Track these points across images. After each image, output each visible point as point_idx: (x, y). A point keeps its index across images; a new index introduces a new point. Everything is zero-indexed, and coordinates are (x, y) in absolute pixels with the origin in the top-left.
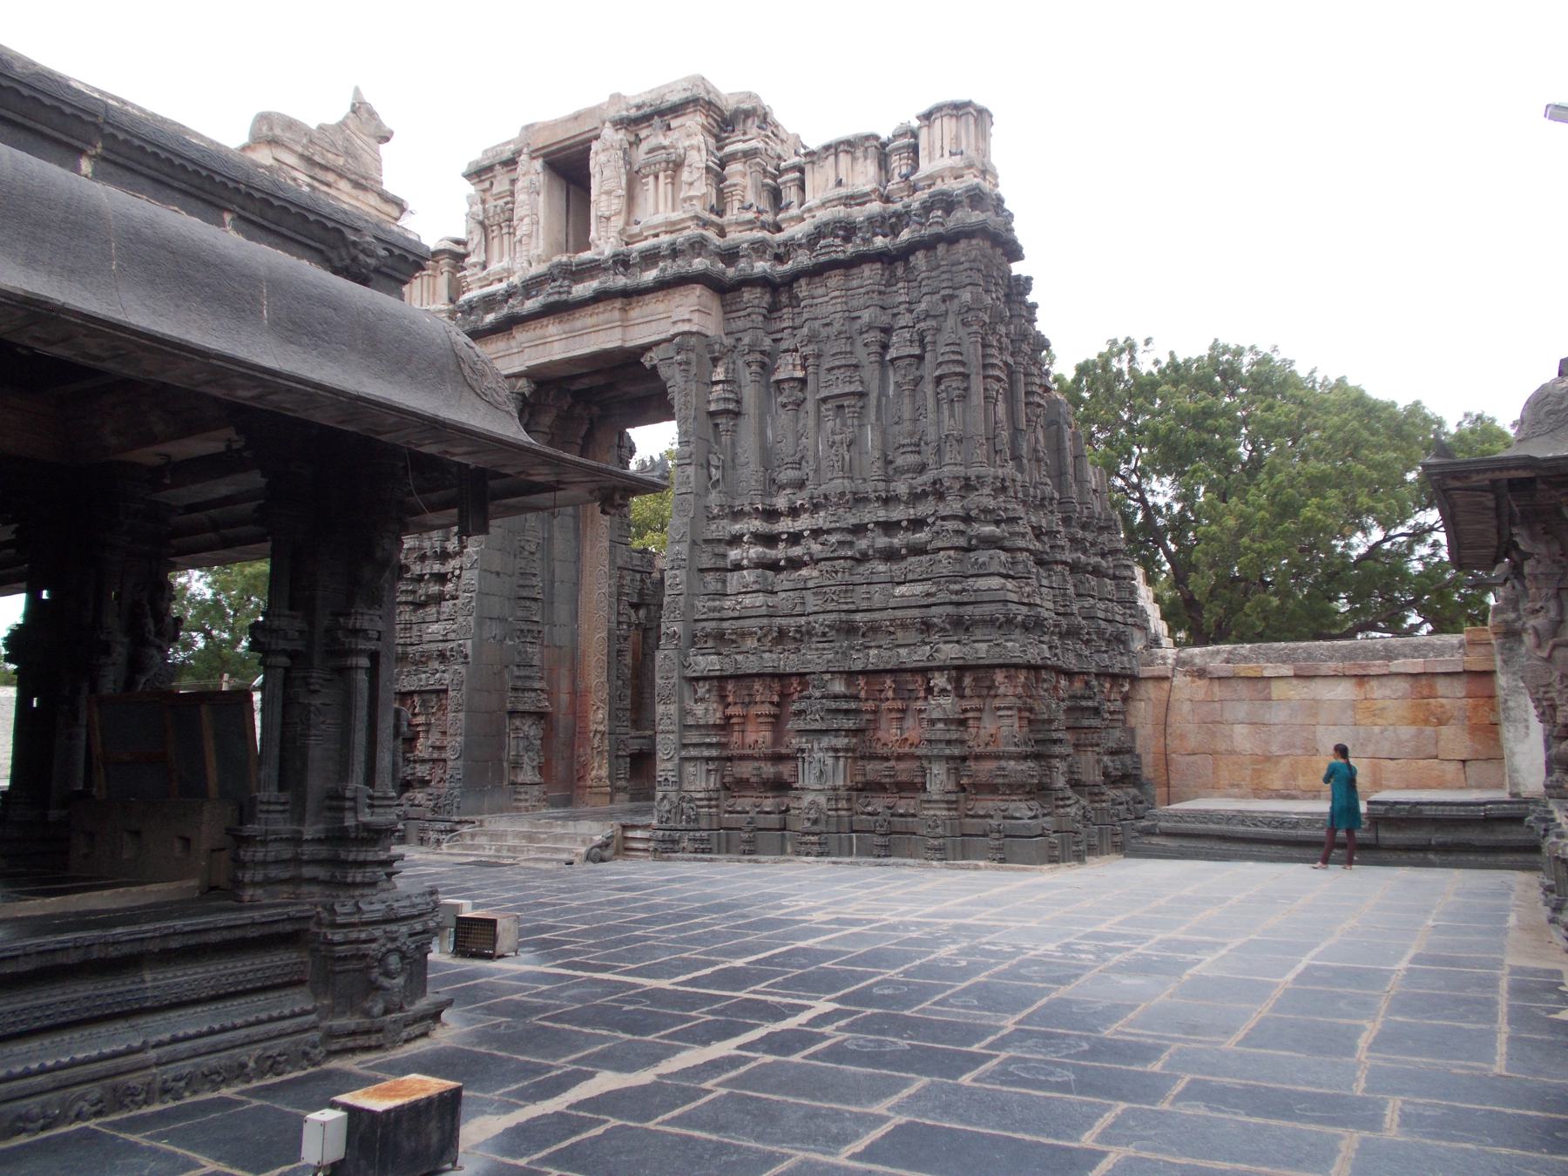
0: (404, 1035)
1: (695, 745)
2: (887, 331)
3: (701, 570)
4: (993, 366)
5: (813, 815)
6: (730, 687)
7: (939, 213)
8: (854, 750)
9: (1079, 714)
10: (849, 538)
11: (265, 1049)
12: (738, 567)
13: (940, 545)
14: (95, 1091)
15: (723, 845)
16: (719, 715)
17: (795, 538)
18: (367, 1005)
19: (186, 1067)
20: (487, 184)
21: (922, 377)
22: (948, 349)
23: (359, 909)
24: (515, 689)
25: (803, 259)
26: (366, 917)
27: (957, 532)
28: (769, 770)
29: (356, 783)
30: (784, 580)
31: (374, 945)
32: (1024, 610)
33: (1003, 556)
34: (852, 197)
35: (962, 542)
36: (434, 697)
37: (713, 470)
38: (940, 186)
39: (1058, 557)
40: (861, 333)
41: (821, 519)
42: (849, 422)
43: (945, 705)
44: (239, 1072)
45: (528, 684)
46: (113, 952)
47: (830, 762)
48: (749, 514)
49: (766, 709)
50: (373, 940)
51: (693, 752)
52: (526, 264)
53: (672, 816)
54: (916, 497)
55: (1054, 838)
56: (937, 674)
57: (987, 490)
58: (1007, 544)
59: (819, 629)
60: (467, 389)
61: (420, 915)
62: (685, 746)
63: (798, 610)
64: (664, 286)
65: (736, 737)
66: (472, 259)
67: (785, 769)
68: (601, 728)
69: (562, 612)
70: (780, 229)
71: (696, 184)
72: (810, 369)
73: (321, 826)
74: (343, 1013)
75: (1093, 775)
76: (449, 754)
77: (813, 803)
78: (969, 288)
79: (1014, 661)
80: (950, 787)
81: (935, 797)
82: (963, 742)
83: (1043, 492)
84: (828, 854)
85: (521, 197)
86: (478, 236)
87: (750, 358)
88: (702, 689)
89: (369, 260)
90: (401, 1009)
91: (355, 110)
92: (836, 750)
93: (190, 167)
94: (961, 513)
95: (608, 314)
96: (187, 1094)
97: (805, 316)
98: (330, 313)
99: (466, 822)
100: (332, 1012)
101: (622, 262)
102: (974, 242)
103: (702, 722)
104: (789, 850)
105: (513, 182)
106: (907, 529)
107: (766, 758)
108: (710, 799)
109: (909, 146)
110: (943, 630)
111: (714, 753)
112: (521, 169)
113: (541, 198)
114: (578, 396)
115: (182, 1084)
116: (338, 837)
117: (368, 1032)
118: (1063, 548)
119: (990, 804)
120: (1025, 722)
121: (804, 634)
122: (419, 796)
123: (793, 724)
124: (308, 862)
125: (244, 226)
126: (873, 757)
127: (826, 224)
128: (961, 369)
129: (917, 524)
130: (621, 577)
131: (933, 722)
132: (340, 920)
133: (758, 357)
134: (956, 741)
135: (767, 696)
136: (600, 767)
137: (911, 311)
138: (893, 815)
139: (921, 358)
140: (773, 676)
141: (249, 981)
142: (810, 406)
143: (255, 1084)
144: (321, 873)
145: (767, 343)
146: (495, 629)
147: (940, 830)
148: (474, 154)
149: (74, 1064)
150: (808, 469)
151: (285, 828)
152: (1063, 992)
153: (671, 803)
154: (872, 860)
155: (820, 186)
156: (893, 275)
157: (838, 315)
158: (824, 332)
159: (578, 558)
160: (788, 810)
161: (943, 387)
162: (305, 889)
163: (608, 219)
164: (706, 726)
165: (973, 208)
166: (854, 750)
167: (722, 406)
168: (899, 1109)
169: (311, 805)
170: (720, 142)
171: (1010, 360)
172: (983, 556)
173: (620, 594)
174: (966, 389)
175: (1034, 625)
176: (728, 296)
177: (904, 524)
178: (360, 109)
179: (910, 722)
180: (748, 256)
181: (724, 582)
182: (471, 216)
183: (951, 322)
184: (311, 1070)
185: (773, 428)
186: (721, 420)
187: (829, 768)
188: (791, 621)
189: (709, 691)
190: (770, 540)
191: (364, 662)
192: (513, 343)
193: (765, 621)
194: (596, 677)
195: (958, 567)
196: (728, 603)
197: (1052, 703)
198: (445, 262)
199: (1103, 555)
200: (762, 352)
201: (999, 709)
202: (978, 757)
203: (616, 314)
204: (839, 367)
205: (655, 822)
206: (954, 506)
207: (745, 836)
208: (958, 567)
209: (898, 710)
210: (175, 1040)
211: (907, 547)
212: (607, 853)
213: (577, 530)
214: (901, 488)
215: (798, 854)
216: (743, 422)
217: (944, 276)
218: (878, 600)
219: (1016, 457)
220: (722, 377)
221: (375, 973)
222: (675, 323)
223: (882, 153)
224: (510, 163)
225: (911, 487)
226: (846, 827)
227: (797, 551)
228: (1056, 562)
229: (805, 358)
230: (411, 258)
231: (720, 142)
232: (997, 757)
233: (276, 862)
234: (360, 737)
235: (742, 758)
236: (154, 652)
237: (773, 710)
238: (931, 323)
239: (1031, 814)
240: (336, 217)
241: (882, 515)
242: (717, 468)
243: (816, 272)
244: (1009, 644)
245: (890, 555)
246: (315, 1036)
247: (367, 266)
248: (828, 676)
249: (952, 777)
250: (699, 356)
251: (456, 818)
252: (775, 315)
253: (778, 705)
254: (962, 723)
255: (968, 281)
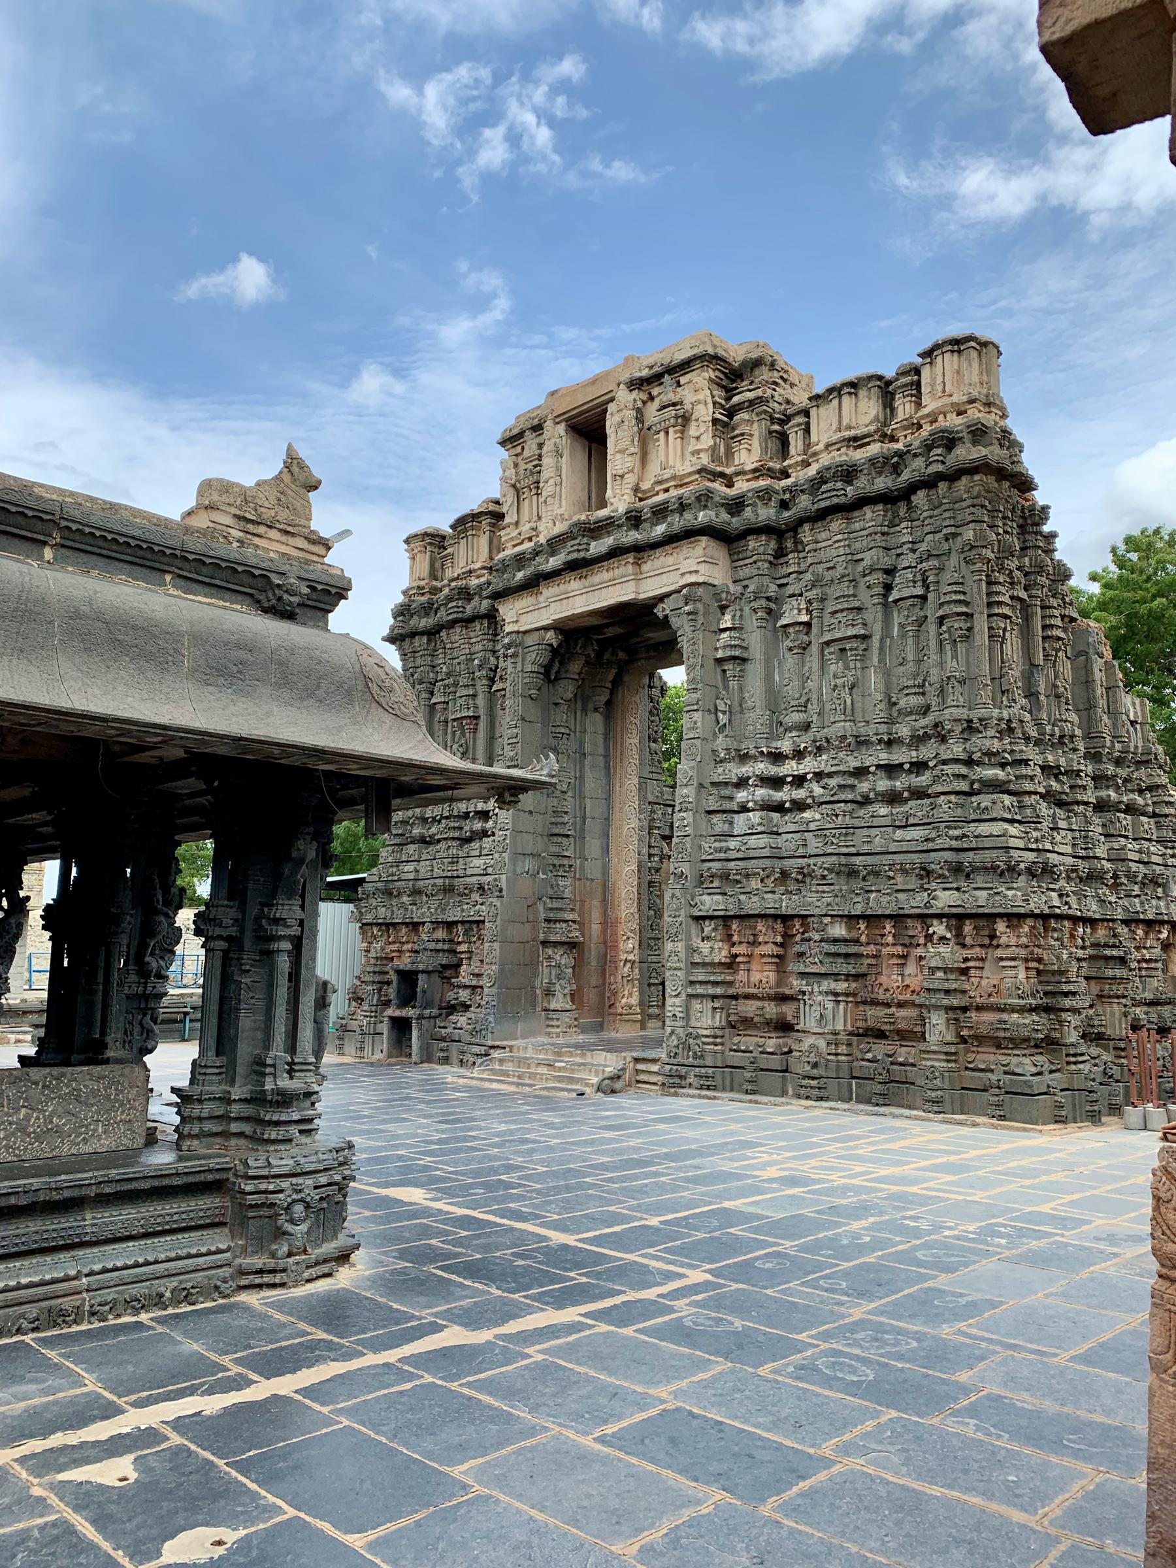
0: (306, 1275)
1: (701, 982)
2: (890, 572)
3: (709, 812)
4: (999, 603)
5: (812, 1059)
6: (734, 927)
7: (939, 451)
8: (855, 995)
9: (1102, 963)
10: (851, 781)
11: (181, 1282)
12: (744, 809)
13: (940, 789)
14: (33, 1311)
15: (728, 1083)
16: (724, 953)
17: (799, 781)
18: (274, 1247)
19: (110, 1294)
20: (519, 449)
21: (926, 617)
22: (950, 589)
23: (269, 1163)
24: (548, 921)
25: (804, 502)
26: (275, 1171)
27: (958, 776)
28: (771, 1010)
29: (277, 1052)
30: (787, 823)
31: (281, 1196)
32: (1031, 856)
33: (1007, 800)
34: (855, 439)
35: (964, 786)
36: (474, 926)
37: (721, 715)
38: (942, 423)
39: (1079, 798)
40: (865, 575)
41: (823, 763)
42: (852, 665)
43: (946, 953)
44: (158, 1301)
45: (560, 915)
46: (56, 1196)
47: (830, 1006)
48: (754, 758)
49: (769, 949)
50: (281, 1191)
51: (700, 990)
52: (550, 524)
53: (680, 1051)
54: (919, 740)
55: (1060, 1097)
56: (935, 922)
57: (991, 732)
58: (1012, 787)
59: (819, 872)
60: (374, 705)
61: (326, 1170)
62: (692, 983)
63: (801, 851)
64: (671, 539)
65: (741, 976)
66: (507, 520)
67: (788, 1010)
68: (631, 957)
69: (593, 847)
70: (788, 476)
71: (702, 435)
72: (815, 613)
73: (245, 1089)
74: (254, 1253)
75: (1119, 1028)
76: (485, 982)
77: (813, 1046)
78: (972, 525)
79: (1015, 910)
80: (949, 1038)
81: (933, 1048)
82: (964, 992)
83: (1062, 729)
84: (827, 1099)
85: (547, 461)
86: (510, 498)
87: (755, 605)
88: (708, 927)
89: (292, 599)
90: (305, 1251)
91: (288, 466)
92: (836, 994)
93: (133, 543)
94: (963, 756)
95: (624, 567)
96: (110, 1317)
97: (810, 561)
98: (242, 654)
99: (498, 1047)
100: (244, 1251)
101: (634, 519)
102: (977, 477)
103: (707, 960)
104: (790, 1092)
105: (540, 446)
106: (910, 771)
107: (770, 998)
108: (715, 1037)
109: (912, 384)
110: (940, 876)
111: (719, 991)
112: (547, 434)
113: (564, 461)
114: (604, 644)
115: (107, 1308)
116: (258, 1099)
117: (273, 1271)
118: (1084, 788)
119: (992, 1058)
120: (1034, 972)
121: (805, 875)
122: (461, 1020)
123: (794, 966)
124: (236, 1119)
125: (182, 583)
126: (875, 1003)
127: (828, 469)
128: (964, 609)
129: (919, 766)
130: (652, 812)
131: (933, 970)
132: (251, 1173)
133: (763, 602)
134: (955, 990)
135: (770, 936)
136: (630, 995)
137: (914, 551)
138: (892, 1063)
139: (924, 598)
140: (775, 917)
141: (167, 1223)
142: (814, 649)
143: (170, 1311)
144: (247, 1128)
145: (772, 589)
146: (529, 864)
147: (937, 1082)
148: (508, 422)
149: (19, 1287)
150: (813, 707)
151: (217, 1089)
152: (942, 1281)
153: (679, 1038)
154: (870, 1108)
155: (825, 425)
156: (895, 515)
157: (840, 559)
158: (828, 576)
159: (608, 796)
160: (790, 1051)
161: (944, 628)
162: (233, 1141)
163: (622, 477)
164: (712, 964)
165: (975, 443)
166: (855, 995)
167: (729, 653)
168: (676, 1394)
169: (241, 1070)
170: (730, 392)
171: (1023, 595)
172: (985, 800)
173: (651, 828)
174: (969, 629)
175: (1043, 872)
176: (735, 545)
177: (907, 766)
178: (293, 463)
179: (911, 969)
180: (754, 505)
181: (731, 823)
182: (504, 480)
183: (954, 560)
184: (221, 1301)
185: (781, 673)
186: (728, 666)
187: (829, 1013)
188: (792, 862)
189: (714, 930)
190: (776, 782)
191: (286, 945)
192: (541, 598)
193: (767, 863)
194: (627, 908)
195: (959, 812)
196: (732, 843)
197: (1066, 952)
198: (486, 522)
199: (1141, 792)
200: (768, 599)
201: (1001, 959)
202: (979, 1008)
203: (630, 568)
204: (842, 611)
205: (664, 1056)
206: (956, 749)
207: (748, 1075)
208: (959, 812)
209: (899, 956)
210: (105, 1271)
211: (909, 789)
212: (618, 1085)
213: (607, 768)
214: (903, 731)
215: (799, 1097)
216: (749, 667)
217: (946, 515)
218: (878, 844)
219: (1032, 695)
220: (729, 625)
221: (281, 1220)
222: (683, 574)
223: (886, 390)
224: (538, 428)
225: (914, 729)
226: (845, 1073)
227: (799, 794)
228: (1078, 803)
229: (809, 602)
230: (333, 591)
231: (730, 392)
232: (1000, 1009)
233: (210, 1118)
234: (281, 1012)
235: (747, 997)
236: (162, 918)
237: (777, 950)
238: (934, 562)
239: (1034, 1070)
240: (262, 565)
241: (884, 757)
242: (724, 713)
243: (821, 516)
244: (1010, 893)
245: (893, 798)
246: (225, 1272)
247: (290, 604)
248: (827, 920)
249: (952, 1027)
250: (706, 606)
251: (490, 1043)
252: (782, 561)
253: (782, 945)
254: (964, 972)
255: (971, 518)
